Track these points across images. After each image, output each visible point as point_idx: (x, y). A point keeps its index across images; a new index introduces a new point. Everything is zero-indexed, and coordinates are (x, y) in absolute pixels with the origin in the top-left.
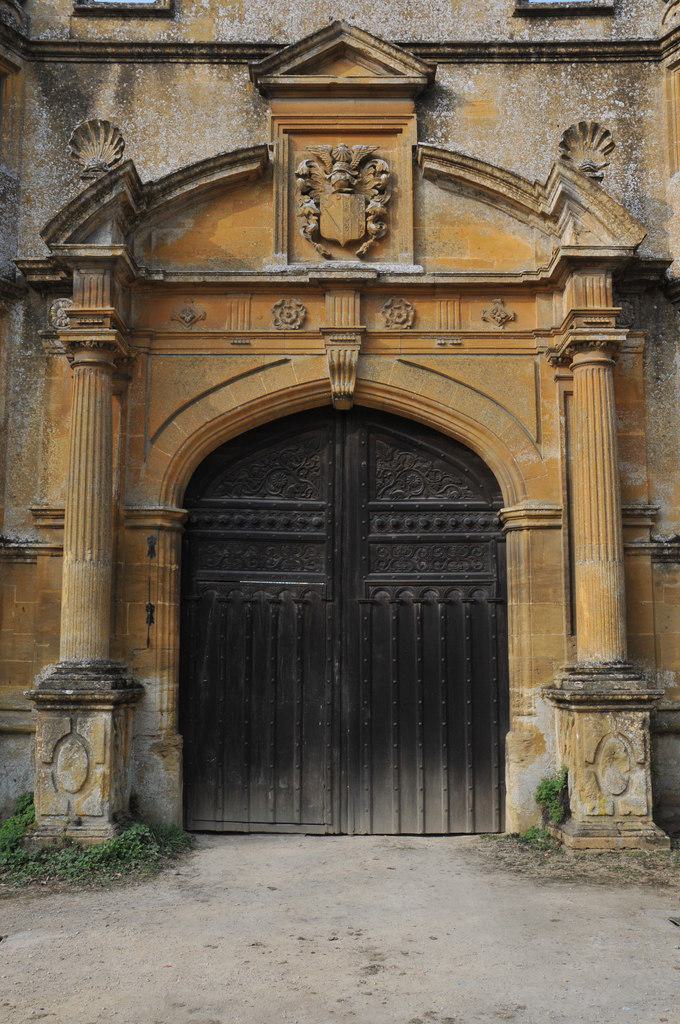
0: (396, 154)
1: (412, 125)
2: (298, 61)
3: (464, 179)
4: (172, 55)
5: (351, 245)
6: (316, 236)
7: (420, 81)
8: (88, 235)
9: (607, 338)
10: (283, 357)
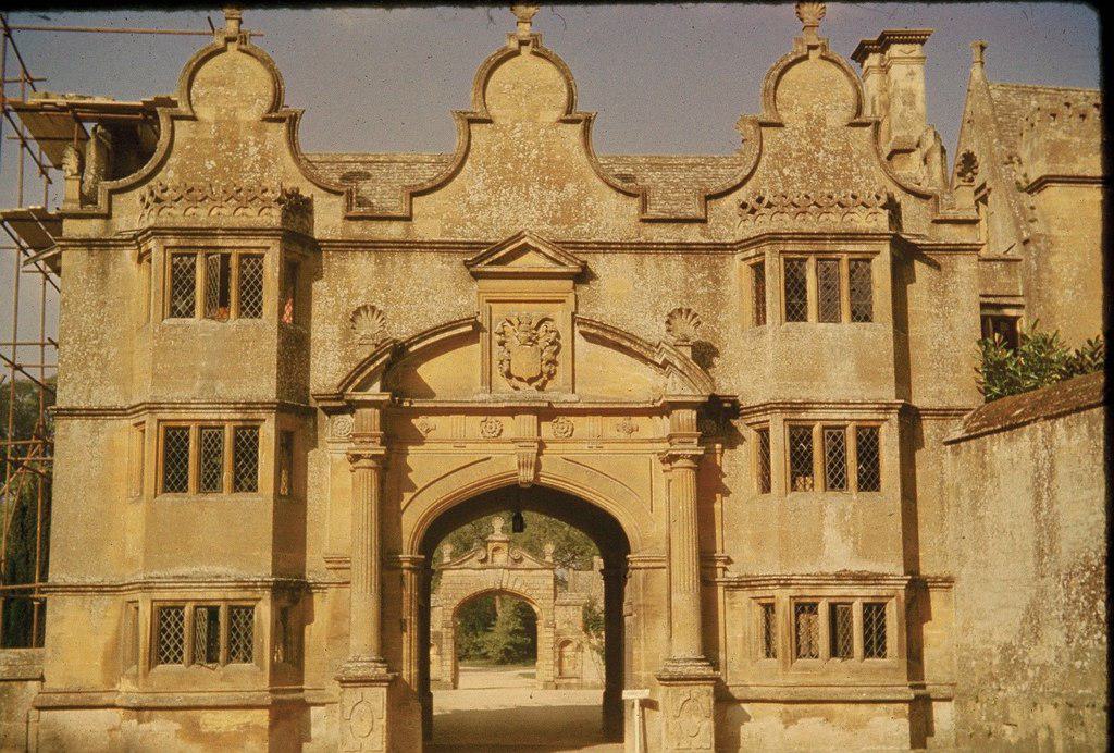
0: (561, 317)
1: (572, 295)
2: (496, 256)
3: (607, 337)
4: (413, 247)
5: (531, 381)
6: (509, 375)
7: (576, 270)
8: (363, 387)
9: (691, 452)
10: (486, 456)
